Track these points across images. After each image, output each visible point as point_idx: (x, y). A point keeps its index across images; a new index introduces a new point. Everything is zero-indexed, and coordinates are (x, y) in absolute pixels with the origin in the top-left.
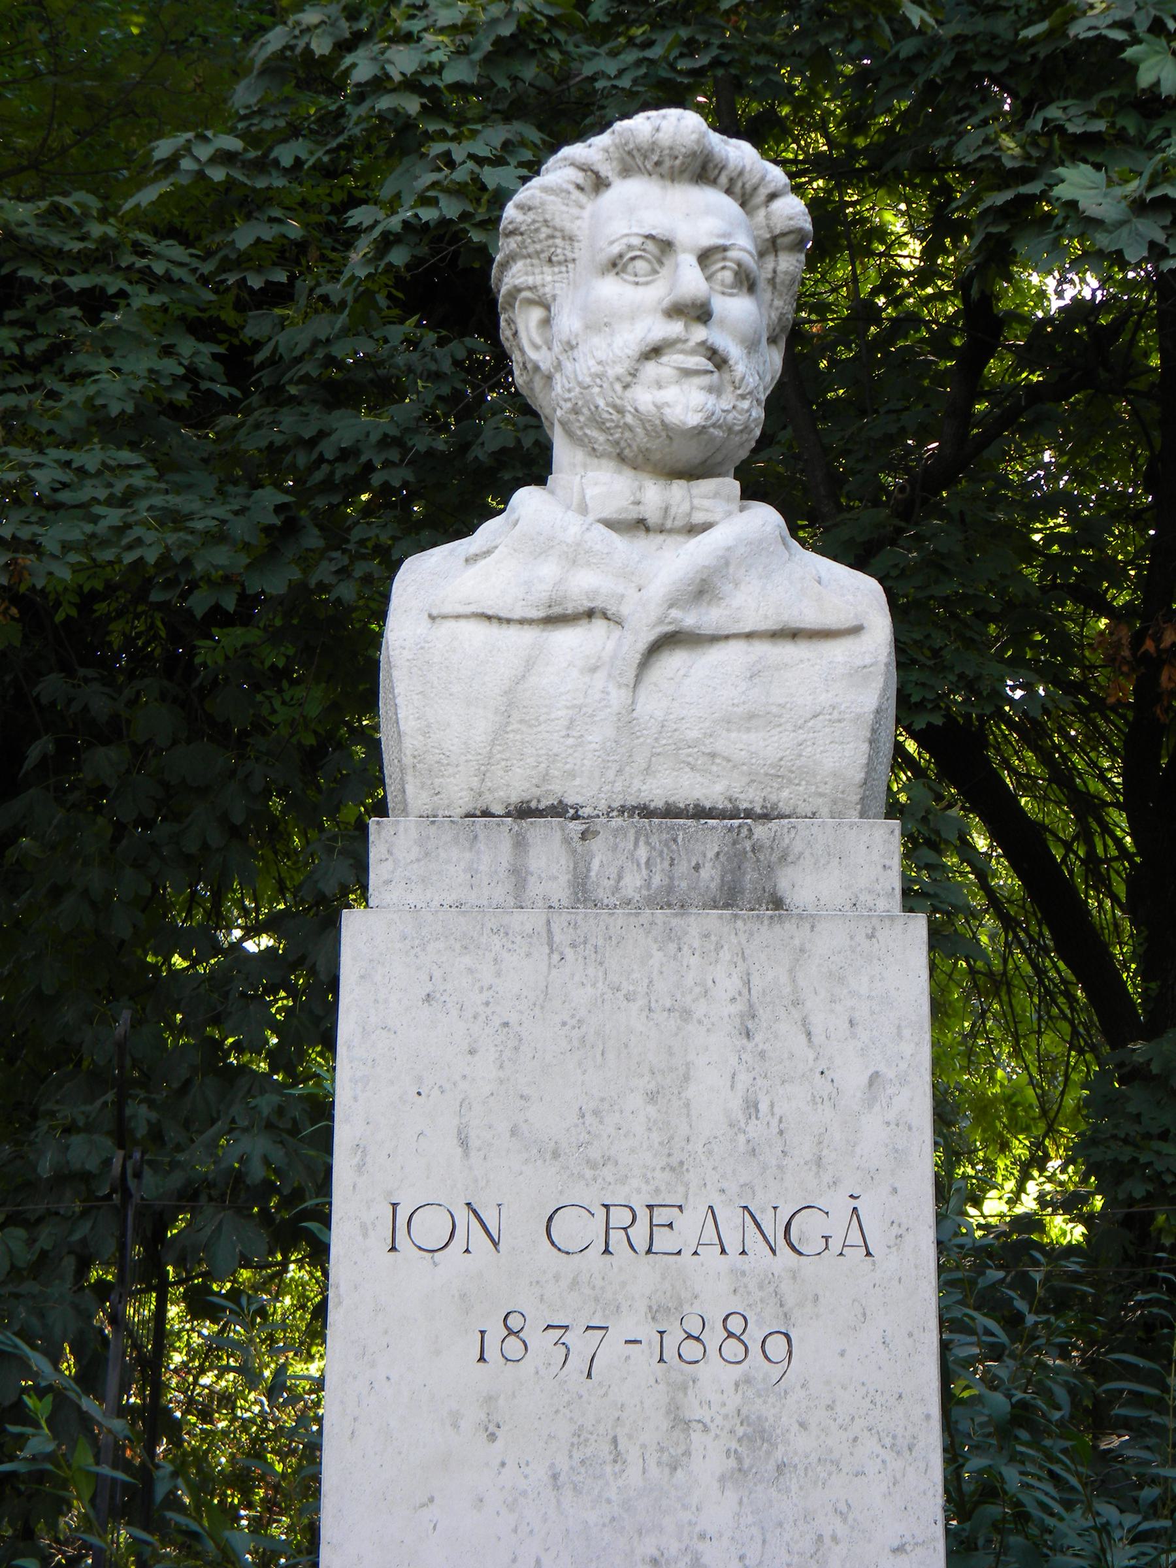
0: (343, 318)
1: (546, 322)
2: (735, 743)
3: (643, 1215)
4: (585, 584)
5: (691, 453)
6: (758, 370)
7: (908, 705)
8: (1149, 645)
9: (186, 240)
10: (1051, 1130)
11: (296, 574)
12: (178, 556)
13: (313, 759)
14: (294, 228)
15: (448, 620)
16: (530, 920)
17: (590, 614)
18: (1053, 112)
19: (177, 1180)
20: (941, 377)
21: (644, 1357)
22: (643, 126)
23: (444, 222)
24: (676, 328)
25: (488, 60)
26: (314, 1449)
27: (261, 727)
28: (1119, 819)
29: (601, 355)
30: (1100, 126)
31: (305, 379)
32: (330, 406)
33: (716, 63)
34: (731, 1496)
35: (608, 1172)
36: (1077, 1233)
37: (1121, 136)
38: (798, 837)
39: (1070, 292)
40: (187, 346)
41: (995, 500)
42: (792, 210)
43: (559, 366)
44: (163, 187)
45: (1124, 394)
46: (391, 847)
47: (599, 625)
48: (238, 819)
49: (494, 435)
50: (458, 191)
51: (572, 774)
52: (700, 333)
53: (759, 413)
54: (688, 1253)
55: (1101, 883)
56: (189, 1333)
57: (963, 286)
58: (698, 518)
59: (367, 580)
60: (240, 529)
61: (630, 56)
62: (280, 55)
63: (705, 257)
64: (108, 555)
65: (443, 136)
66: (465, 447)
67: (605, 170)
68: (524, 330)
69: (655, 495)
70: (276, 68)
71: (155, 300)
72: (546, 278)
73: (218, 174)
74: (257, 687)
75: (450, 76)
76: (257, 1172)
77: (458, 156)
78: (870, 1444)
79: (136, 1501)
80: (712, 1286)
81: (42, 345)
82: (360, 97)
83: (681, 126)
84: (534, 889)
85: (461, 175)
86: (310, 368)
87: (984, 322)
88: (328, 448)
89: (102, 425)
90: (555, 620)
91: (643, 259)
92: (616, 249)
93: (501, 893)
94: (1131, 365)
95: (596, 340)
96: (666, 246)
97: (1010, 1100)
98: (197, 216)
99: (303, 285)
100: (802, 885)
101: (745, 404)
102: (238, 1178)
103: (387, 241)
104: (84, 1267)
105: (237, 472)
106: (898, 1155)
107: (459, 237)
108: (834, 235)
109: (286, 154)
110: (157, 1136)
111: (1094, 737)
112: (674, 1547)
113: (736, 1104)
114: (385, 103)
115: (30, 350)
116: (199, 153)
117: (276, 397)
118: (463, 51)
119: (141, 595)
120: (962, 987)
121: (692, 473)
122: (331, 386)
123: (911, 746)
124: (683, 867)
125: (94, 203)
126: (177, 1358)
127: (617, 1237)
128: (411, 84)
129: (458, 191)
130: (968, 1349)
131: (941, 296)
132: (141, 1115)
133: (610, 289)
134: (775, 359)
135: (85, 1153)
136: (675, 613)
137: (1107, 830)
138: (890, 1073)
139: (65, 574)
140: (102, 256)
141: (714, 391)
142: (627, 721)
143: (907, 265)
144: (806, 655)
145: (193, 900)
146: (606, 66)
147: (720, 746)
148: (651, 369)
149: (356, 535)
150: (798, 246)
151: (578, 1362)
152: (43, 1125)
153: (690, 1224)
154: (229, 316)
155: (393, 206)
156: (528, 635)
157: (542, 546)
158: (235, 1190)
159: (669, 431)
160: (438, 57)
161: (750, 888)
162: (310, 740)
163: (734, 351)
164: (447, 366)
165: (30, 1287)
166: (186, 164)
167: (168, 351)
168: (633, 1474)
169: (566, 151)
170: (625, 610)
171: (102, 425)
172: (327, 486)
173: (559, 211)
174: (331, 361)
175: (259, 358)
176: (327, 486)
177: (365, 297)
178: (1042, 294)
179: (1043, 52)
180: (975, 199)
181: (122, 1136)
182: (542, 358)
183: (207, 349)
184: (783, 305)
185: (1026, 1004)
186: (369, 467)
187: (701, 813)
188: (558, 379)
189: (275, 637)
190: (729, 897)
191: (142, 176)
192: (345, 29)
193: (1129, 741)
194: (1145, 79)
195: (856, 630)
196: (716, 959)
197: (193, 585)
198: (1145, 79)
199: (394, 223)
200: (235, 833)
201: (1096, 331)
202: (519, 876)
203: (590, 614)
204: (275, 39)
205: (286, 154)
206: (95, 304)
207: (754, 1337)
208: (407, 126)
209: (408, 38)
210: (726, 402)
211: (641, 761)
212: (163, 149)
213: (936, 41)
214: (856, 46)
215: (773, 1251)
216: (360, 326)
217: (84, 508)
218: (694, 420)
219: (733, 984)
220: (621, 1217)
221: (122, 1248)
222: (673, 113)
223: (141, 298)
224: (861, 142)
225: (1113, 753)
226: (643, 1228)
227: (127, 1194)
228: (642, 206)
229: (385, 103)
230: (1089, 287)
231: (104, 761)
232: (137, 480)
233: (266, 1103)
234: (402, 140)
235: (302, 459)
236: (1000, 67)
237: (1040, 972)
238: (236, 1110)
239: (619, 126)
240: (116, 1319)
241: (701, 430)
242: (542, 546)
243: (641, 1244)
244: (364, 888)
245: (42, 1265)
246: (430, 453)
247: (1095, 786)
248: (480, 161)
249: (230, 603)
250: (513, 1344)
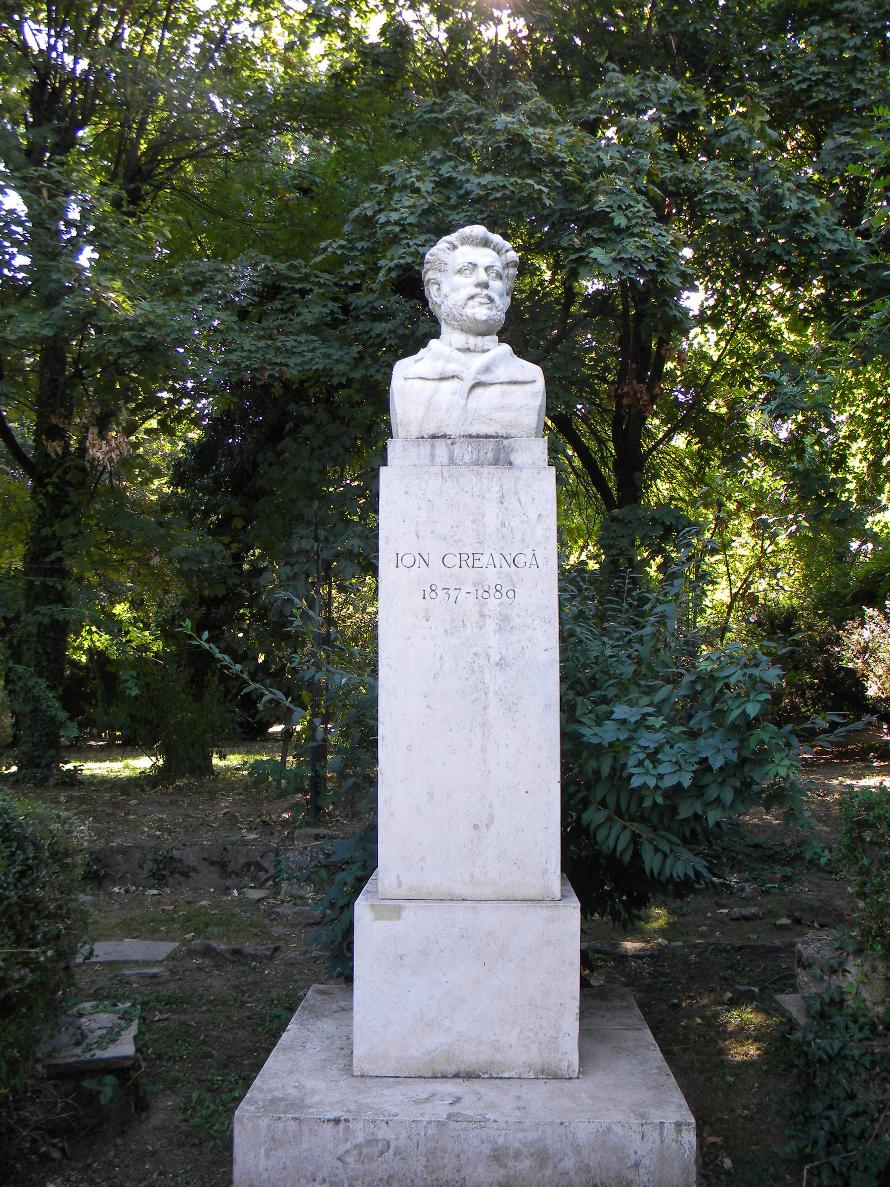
0: (376, 295)
1: (439, 289)
2: (497, 415)
3: (471, 556)
4: (451, 368)
5: (483, 328)
6: (503, 303)
7: (550, 410)
8: (620, 391)
9: (329, 273)
10: (590, 537)
11: (363, 372)
12: (328, 367)
13: (369, 428)
14: (362, 267)
16: (436, 469)
17: (453, 377)
18: (590, 231)
19: (333, 552)
20: (557, 312)
21: (471, 597)
22: (468, 230)
23: (408, 264)
24: (478, 290)
25: (420, 216)
26: (376, 627)
27: (353, 419)
28: (611, 445)
30: (603, 236)
31: (366, 313)
32: (373, 321)
33: (489, 216)
34: (497, 636)
35: (460, 544)
36: (597, 566)
37: (610, 239)
38: (516, 444)
39: (595, 287)
40: (331, 304)
41: (574, 348)
44: (323, 256)
45: (611, 317)
46: (394, 448)
47: (456, 380)
48: (347, 445)
49: (423, 328)
50: (411, 254)
51: (448, 426)
52: (485, 292)
53: (504, 316)
55: (605, 464)
56: (338, 597)
57: (563, 284)
58: (486, 348)
59: (385, 373)
60: (347, 358)
61: (462, 215)
62: (357, 216)
63: (487, 269)
64: (308, 367)
65: (406, 238)
66: (413, 333)
67: (456, 243)
68: (432, 292)
69: (472, 341)
70: (356, 220)
71: (321, 291)
72: (438, 276)
73: (339, 252)
74: (353, 407)
75: (408, 221)
76: (356, 550)
77: (411, 243)
78: (538, 621)
79: (326, 640)
80: (491, 577)
81: (288, 305)
82: (381, 228)
83: (479, 230)
84: (437, 460)
85: (412, 250)
86: (367, 310)
87: (570, 294)
88: (373, 334)
89: (305, 329)
90: (442, 379)
91: (468, 270)
93: (427, 461)
94: (613, 308)
96: (475, 266)
97: (578, 528)
98: (335, 263)
99: (364, 286)
100: (518, 458)
102: (351, 551)
103: (390, 270)
104: (308, 577)
105: (346, 342)
106: (547, 538)
107: (412, 268)
108: (524, 268)
109: (359, 245)
110: (327, 540)
111: (604, 421)
112: (481, 651)
113: (499, 523)
114: (389, 228)
115: (285, 307)
116: (333, 246)
117: (357, 319)
118: (412, 213)
119: (318, 380)
120: (566, 496)
121: (484, 334)
122: (373, 315)
123: (549, 423)
124: (482, 453)
125: (303, 263)
126: (335, 605)
128: (397, 223)
129: (411, 254)
130: (567, 596)
131: (557, 287)
132: (322, 533)
133: (458, 279)
134: (508, 300)
135: (306, 544)
137: (607, 448)
138: (544, 514)
139: (296, 373)
140: (305, 278)
141: (491, 309)
142: (465, 409)
143: (547, 278)
144: (519, 390)
145: (335, 471)
146: (454, 217)
147: (493, 416)
148: (471, 303)
149: (381, 360)
150: (514, 266)
151: (452, 599)
152: (294, 536)
153: (485, 559)
154: (343, 296)
155: (392, 260)
156: (434, 383)
157: (438, 357)
158: (350, 555)
159: (476, 321)
160: (405, 215)
161: (502, 459)
162: (368, 422)
164: (408, 308)
165: (292, 583)
166: (330, 249)
167: (325, 306)
168: (469, 631)
169: (445, 238)
170: (464, 375)
171: (305, 329)
172: (373, 345)
173: (442, 256)
174: (374, 308)
175: (352, 307)
176: (373, 345)
177: (383, 285)
178: (587, 287)
179: (586, 214)
180: (567, 257)
181: (317, 539)
182: (438, 300)
183: (337, 305)
184: (510, 284)
185: (584, 500)
186: (385, 339)
187: (487, 437)
188: (443, 307)
189: (357, 391)
190: (496, 462)
191: (316, 253)
192: (377, 207)
193: (614, 421)
194: (616, 223)
195: (534, 381)
196: (492, 481)
197: (333, 376)
198: (616, 223)
199: (392, 264)
200: (347, 450)
201: (603, 297)
202: (433, 456)
203: (453, 377)
204: (356, 211)
205: (359, 245)
206: (303, 293)
207: (504, 591)
208: (396, 236)
209: (396, 210)
210: (494, 312)
211: (469, 421)
212: (323, 245)
213: (555, 210)
214: (530, 212)
216: (382, 296)
217: (301, 354)
218: (484, 318)
219: (498, 488)
220: (464, 557)
221: (318, 572)
222: (477, 226)
223: (317, 290)
224: (532, 241)
225: (609, 425)
226: (470, 560)
227: (319, 556)
228: (467, 254)
229: (389, 228)
230: (600, 286)
231: (308, 429)
232: (316, 344)
233: (358, 529)
234: (394, 240)
235: (365, 337)
236: (573, 218)
237: (587, 490)
238: (350, 532)
239: (461, 230)
240: (317, 592)
241: (486, 321)
242: (438, 357)
243: (471, 565)
245: (295, 576)
246: (404, 335)
247: (604, 435)
248: (418, 245)
249: (344, 381)
250: (433, 594)
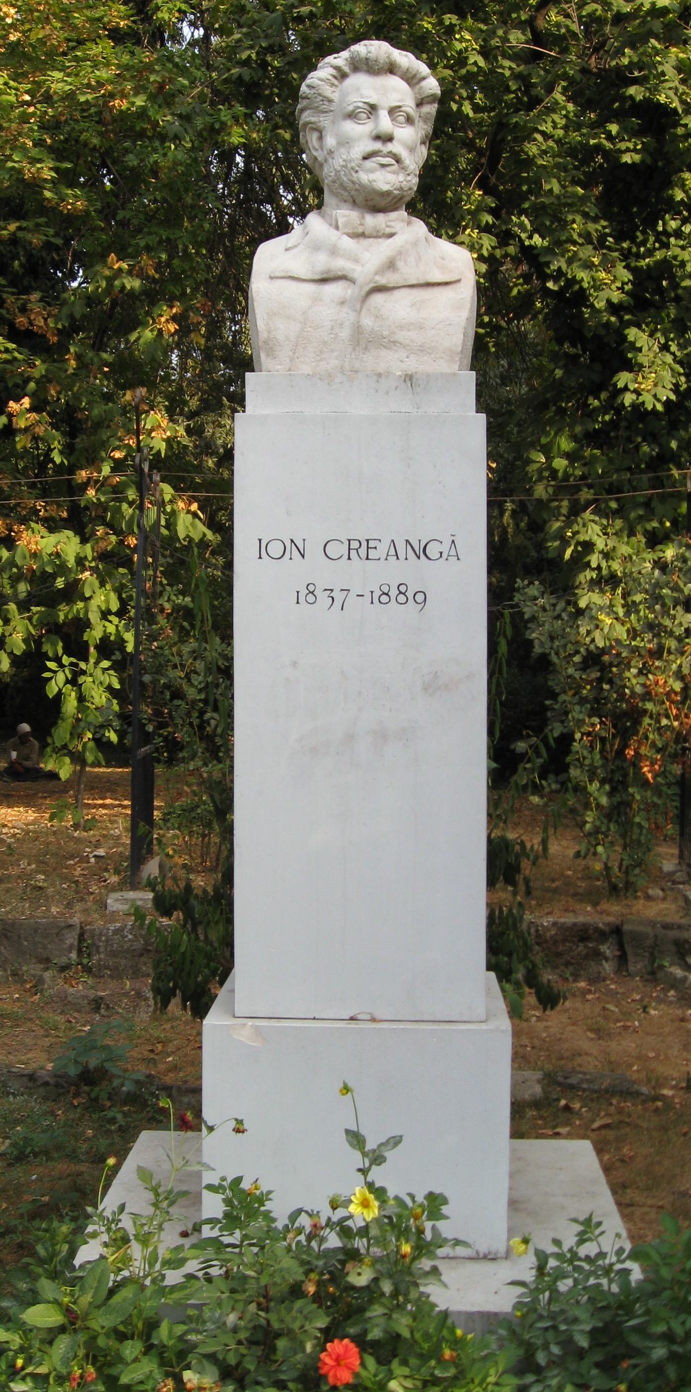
1: (321, 138)
3: (364, 544)
4: (340, 264)
15: (279, 271)
24: (378, 146)
29: (344, 157)
42: (432, 85)
43: (326, 161)
53: (415, 180)
54: (383, 559)
63: (392, 111)
67: (346, 69)
92: (351, 108)
95: (343, 150)
101: (409, 178)
127: (353, 553)
136: (377, 278)
148: (368, 164)
156: (311, 288)
163: (404, 154)
170: (355, 276)
173: (327, 91)
207: (410, 595)
215: (292, 541)
220: (354, 545)
222: (376, 43)
228: (364, 88)
243: (363, 555)
244: (244, 407)
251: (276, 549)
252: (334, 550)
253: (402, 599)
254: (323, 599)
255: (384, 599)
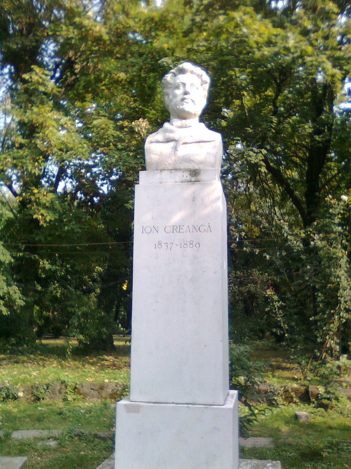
127: (174, 230)
207: (194, 244)
220: (175, 227)
251: (148, 230)
252: (168, 229)
253: (191, 246)
254: (164, 246)
255: (185, 246)
